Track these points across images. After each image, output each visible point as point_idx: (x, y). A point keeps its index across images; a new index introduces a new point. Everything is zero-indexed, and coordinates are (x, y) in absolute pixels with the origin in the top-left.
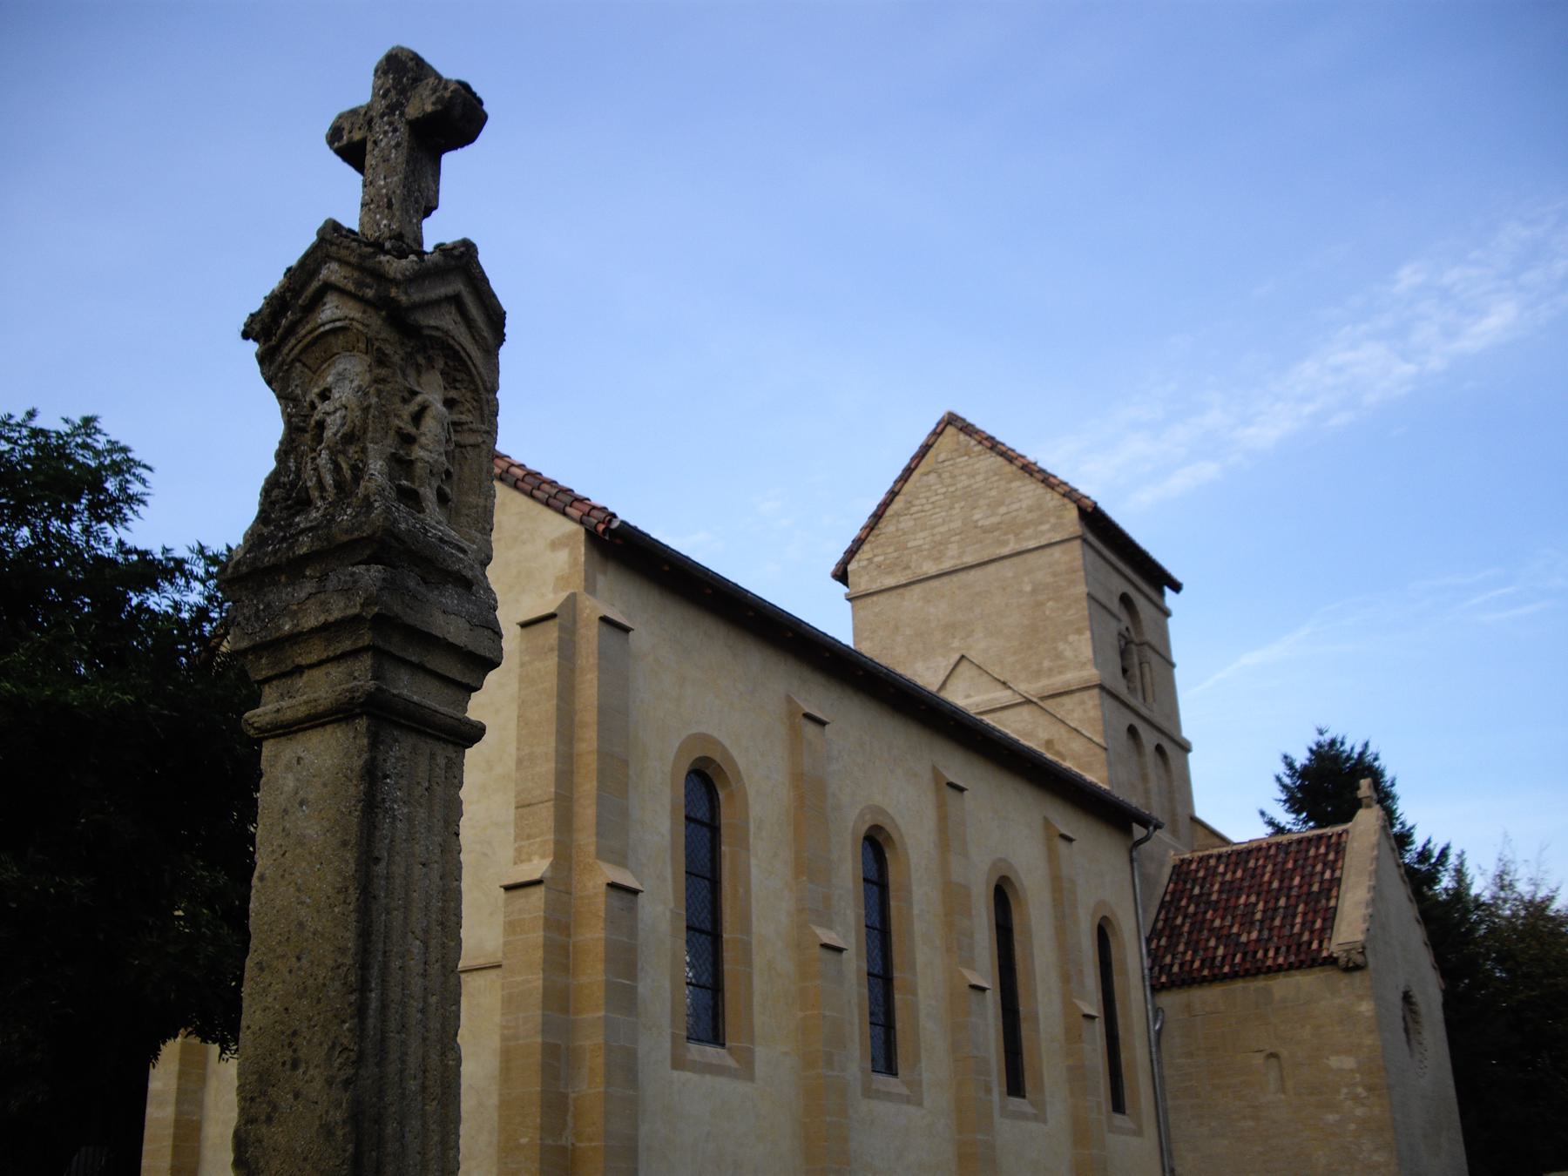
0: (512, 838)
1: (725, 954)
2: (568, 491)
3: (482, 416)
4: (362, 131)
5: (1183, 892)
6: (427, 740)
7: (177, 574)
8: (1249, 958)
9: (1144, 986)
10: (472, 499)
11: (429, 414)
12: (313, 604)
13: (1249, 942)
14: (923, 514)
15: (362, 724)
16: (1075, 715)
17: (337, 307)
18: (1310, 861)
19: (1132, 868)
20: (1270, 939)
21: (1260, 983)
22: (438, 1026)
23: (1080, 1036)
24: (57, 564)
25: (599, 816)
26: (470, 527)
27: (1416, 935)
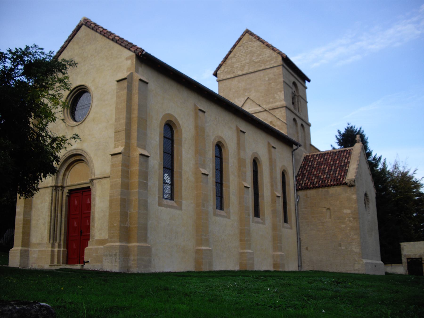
1: (174, 175)
2: (131, 44)
5: (306, 164)
8: (323, 182)
9: (294, 189)
13: (324, 178)
16: (279, 115)
18: (342, 157)
19: (293, 157)
20: (329, 177)
21: (326, 189)
23: (276, 201)
25: (138, 135)
27: (369, 178)
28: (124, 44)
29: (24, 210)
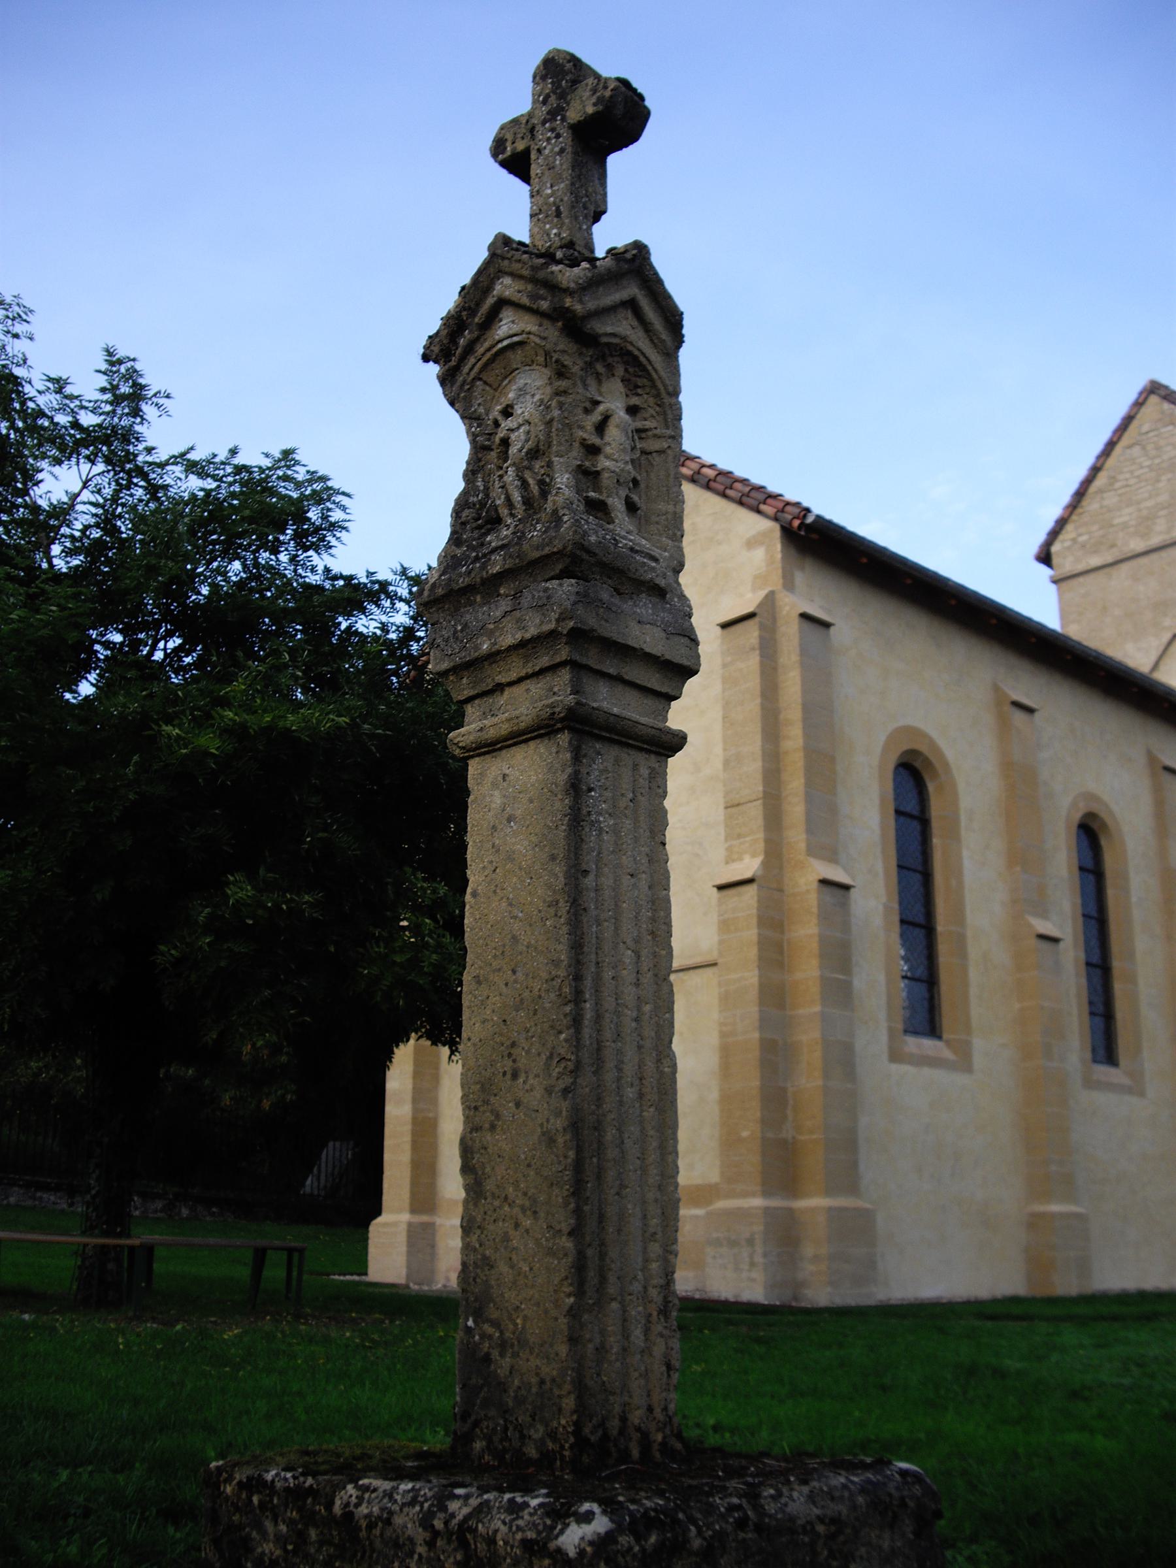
0: (722, 837)
2: (760, 489)
3: (666, 420)
4: (525, 141)
6: (629, 751)
7: (383, 597)
10: (662, 506)
11: (612, 422)
12: (509, 622)
14: (1128, 489)
15: (564, 738)
17: (513, 322)
22: (653, 1034)
24: (269, 594)
25: (808, 813)
26: (661, 535)
28: (736, 490)
29: (415, 1085)
